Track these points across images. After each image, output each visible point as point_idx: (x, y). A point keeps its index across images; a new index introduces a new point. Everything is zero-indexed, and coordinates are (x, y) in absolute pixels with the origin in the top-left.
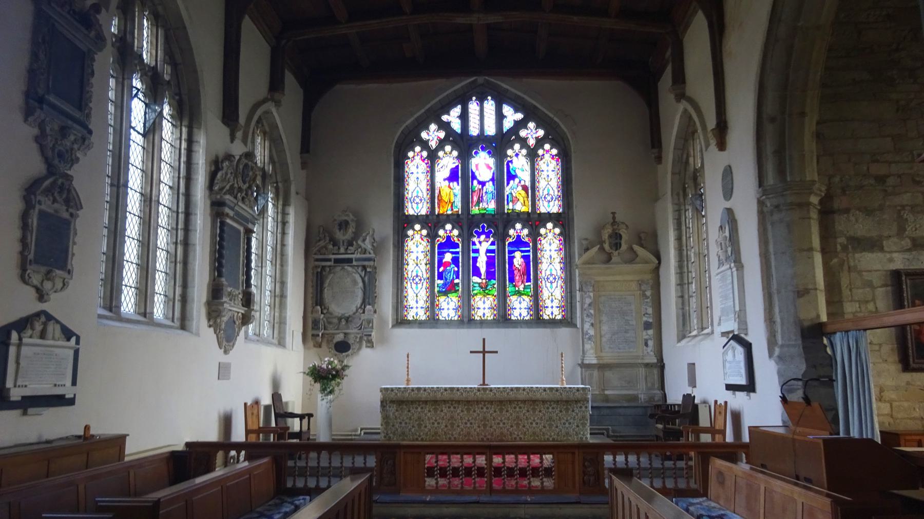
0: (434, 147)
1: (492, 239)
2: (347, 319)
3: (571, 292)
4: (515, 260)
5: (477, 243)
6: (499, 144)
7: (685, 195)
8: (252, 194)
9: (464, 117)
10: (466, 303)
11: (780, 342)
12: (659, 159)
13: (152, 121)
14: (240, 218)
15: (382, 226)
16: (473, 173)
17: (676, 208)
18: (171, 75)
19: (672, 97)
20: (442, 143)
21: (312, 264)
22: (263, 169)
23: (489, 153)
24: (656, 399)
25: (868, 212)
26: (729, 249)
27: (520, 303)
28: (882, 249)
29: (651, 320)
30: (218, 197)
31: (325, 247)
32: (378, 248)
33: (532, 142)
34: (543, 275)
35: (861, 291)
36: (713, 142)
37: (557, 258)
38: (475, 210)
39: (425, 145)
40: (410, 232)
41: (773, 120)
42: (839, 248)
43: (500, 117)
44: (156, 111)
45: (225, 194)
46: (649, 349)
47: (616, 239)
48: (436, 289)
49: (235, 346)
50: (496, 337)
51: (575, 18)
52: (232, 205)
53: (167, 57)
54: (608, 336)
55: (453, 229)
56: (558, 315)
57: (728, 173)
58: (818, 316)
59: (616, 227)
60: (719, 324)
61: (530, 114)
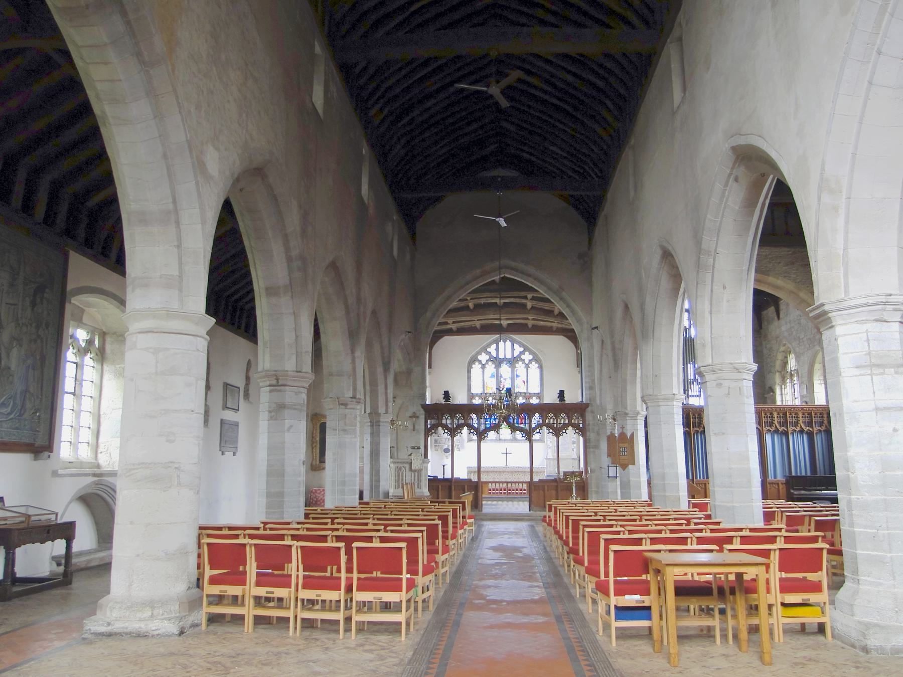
6: (513, 362)
9: (497, 349)
39: (480, 362)
43: (513, 349)
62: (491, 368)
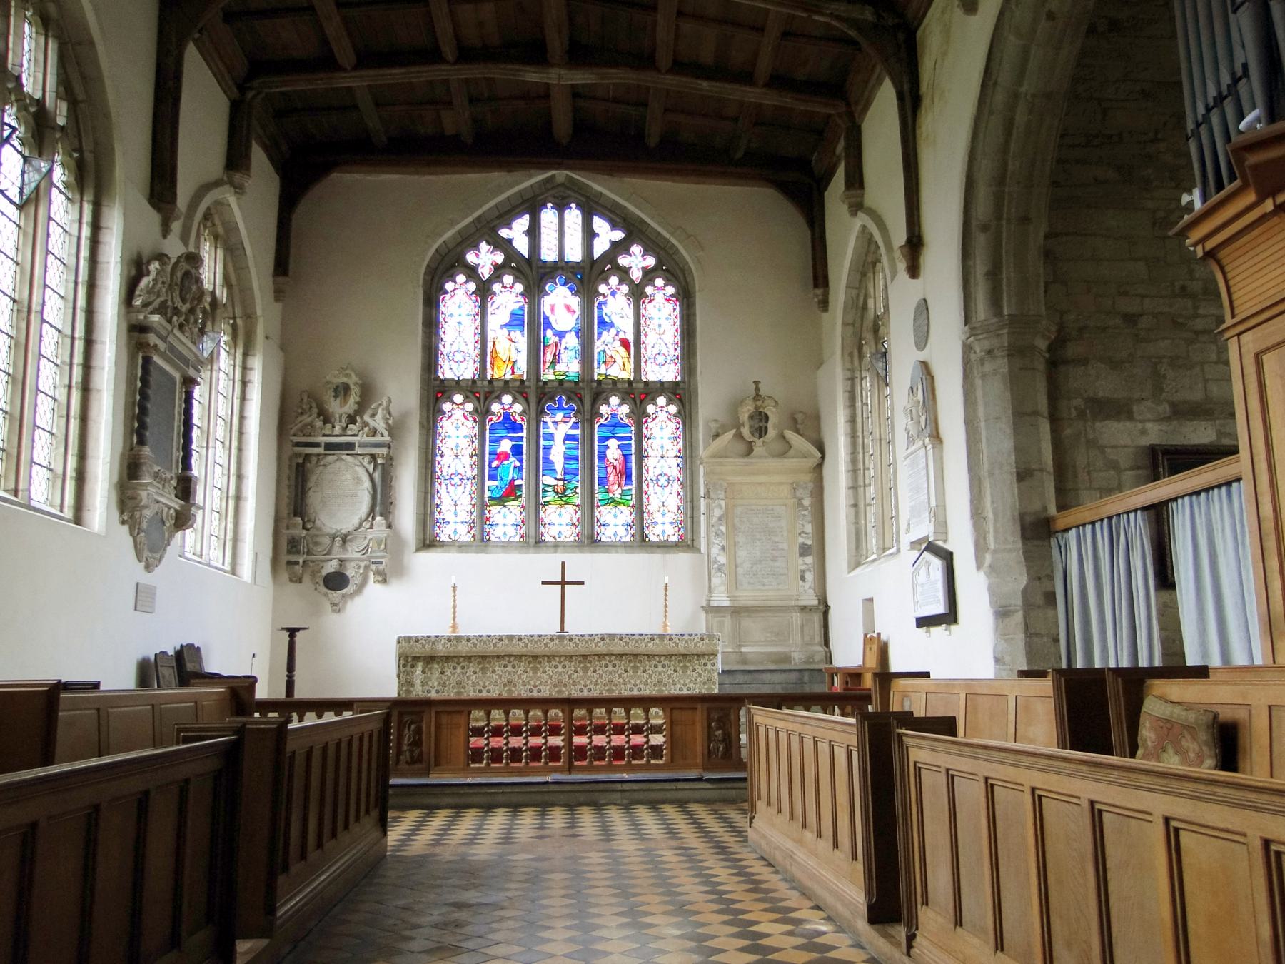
0: (487, 276)
1: (574, 420)
2: (345, 539)
3: (692, 501)
4: (608, 452)
5: (550, 425)
6: (587, 276)
7: (861, 356)
8: (196, 321)
9: (534, 232)
10: (532, 516)
11: (992, 546)
12: (824, 304)
13: (33, 185)
14: (175, 355)
15: (401, 391)
16: (546, 318)
17: (849, 374)
18: (68, 117)
19: (844, 208)
20: (498, 271)
21: (289, 449)
22: (213, 293)
23: (571, 289)
24: (817, 658)
25: (1115, 365)
26: (923, 418)
27: (615, 516)
28: (1130, 417)
29: (809, 542)
30: (141, 317)
31: (311, 425)
32: (395, 430)
33: (636, 275)
34: (649, 475)
35: (1103, 474)
36: (902, 266)
37: (673, 449)
38: (548, 375)
39: (472, 272)
40: (447, 407)
41: (985, 228)
42: (1074, 413)
43: (589, 235)
44: (38, 170)
45: (152, 313)
46: (807, 585)
47: (760, 422)
48: (487, 494)
49: (164, 561)
50: (579, 564)
51: (705, 84)
52: (164, 333)
53: (61, 89)
54: (747, 565)
55: (514, 402)
56: (673, 535)
57: (923, 309)
58: (1045, 509)
59: (759, 403)
60: (908, 531)
61: (634, 232)
62: (508, 298)
